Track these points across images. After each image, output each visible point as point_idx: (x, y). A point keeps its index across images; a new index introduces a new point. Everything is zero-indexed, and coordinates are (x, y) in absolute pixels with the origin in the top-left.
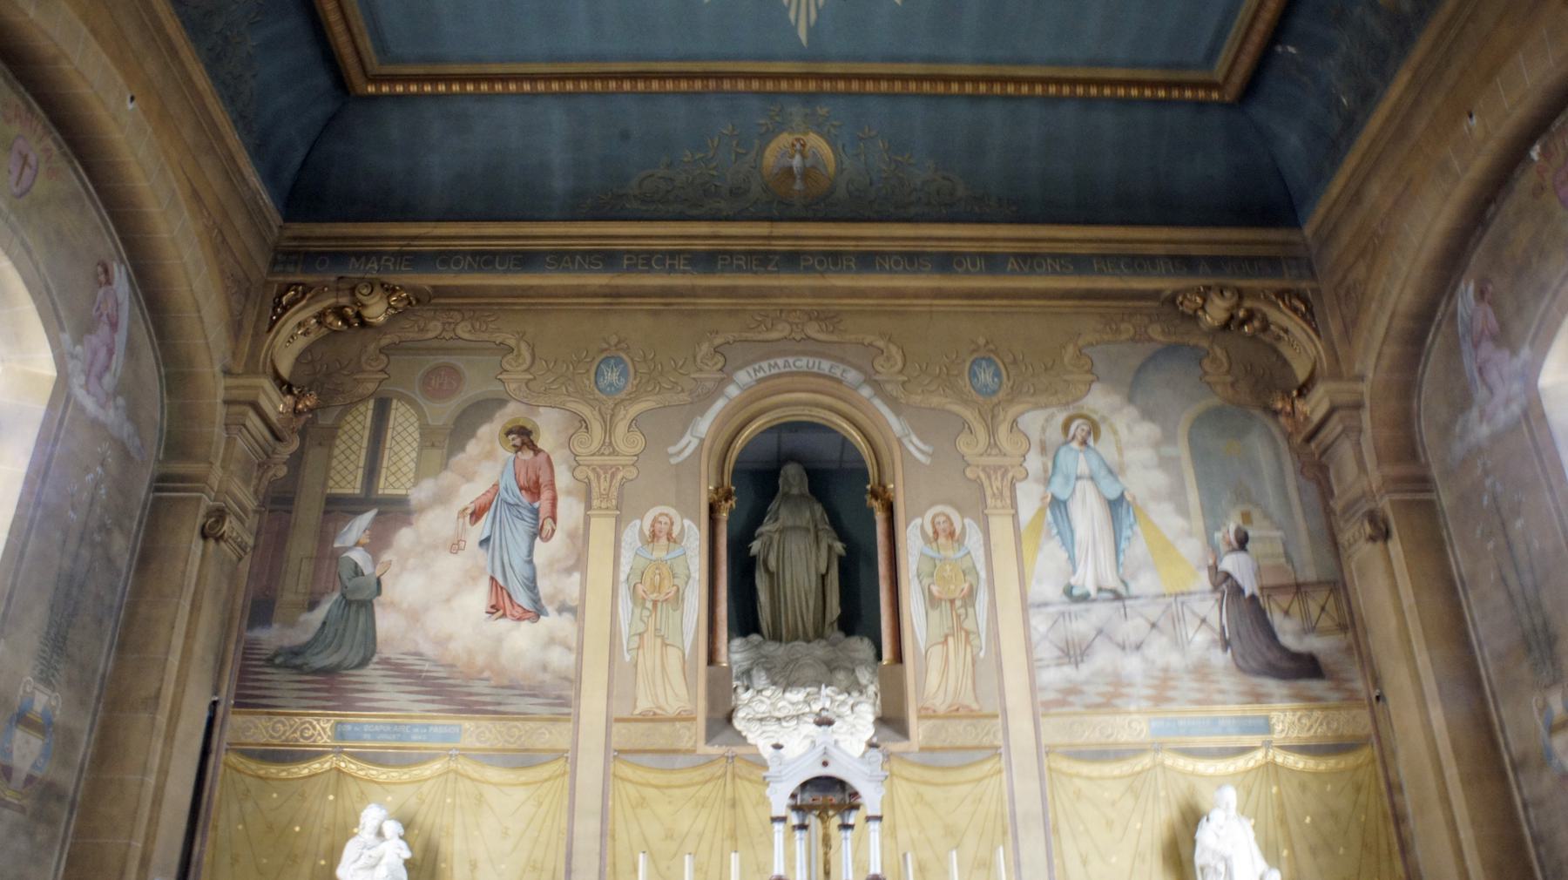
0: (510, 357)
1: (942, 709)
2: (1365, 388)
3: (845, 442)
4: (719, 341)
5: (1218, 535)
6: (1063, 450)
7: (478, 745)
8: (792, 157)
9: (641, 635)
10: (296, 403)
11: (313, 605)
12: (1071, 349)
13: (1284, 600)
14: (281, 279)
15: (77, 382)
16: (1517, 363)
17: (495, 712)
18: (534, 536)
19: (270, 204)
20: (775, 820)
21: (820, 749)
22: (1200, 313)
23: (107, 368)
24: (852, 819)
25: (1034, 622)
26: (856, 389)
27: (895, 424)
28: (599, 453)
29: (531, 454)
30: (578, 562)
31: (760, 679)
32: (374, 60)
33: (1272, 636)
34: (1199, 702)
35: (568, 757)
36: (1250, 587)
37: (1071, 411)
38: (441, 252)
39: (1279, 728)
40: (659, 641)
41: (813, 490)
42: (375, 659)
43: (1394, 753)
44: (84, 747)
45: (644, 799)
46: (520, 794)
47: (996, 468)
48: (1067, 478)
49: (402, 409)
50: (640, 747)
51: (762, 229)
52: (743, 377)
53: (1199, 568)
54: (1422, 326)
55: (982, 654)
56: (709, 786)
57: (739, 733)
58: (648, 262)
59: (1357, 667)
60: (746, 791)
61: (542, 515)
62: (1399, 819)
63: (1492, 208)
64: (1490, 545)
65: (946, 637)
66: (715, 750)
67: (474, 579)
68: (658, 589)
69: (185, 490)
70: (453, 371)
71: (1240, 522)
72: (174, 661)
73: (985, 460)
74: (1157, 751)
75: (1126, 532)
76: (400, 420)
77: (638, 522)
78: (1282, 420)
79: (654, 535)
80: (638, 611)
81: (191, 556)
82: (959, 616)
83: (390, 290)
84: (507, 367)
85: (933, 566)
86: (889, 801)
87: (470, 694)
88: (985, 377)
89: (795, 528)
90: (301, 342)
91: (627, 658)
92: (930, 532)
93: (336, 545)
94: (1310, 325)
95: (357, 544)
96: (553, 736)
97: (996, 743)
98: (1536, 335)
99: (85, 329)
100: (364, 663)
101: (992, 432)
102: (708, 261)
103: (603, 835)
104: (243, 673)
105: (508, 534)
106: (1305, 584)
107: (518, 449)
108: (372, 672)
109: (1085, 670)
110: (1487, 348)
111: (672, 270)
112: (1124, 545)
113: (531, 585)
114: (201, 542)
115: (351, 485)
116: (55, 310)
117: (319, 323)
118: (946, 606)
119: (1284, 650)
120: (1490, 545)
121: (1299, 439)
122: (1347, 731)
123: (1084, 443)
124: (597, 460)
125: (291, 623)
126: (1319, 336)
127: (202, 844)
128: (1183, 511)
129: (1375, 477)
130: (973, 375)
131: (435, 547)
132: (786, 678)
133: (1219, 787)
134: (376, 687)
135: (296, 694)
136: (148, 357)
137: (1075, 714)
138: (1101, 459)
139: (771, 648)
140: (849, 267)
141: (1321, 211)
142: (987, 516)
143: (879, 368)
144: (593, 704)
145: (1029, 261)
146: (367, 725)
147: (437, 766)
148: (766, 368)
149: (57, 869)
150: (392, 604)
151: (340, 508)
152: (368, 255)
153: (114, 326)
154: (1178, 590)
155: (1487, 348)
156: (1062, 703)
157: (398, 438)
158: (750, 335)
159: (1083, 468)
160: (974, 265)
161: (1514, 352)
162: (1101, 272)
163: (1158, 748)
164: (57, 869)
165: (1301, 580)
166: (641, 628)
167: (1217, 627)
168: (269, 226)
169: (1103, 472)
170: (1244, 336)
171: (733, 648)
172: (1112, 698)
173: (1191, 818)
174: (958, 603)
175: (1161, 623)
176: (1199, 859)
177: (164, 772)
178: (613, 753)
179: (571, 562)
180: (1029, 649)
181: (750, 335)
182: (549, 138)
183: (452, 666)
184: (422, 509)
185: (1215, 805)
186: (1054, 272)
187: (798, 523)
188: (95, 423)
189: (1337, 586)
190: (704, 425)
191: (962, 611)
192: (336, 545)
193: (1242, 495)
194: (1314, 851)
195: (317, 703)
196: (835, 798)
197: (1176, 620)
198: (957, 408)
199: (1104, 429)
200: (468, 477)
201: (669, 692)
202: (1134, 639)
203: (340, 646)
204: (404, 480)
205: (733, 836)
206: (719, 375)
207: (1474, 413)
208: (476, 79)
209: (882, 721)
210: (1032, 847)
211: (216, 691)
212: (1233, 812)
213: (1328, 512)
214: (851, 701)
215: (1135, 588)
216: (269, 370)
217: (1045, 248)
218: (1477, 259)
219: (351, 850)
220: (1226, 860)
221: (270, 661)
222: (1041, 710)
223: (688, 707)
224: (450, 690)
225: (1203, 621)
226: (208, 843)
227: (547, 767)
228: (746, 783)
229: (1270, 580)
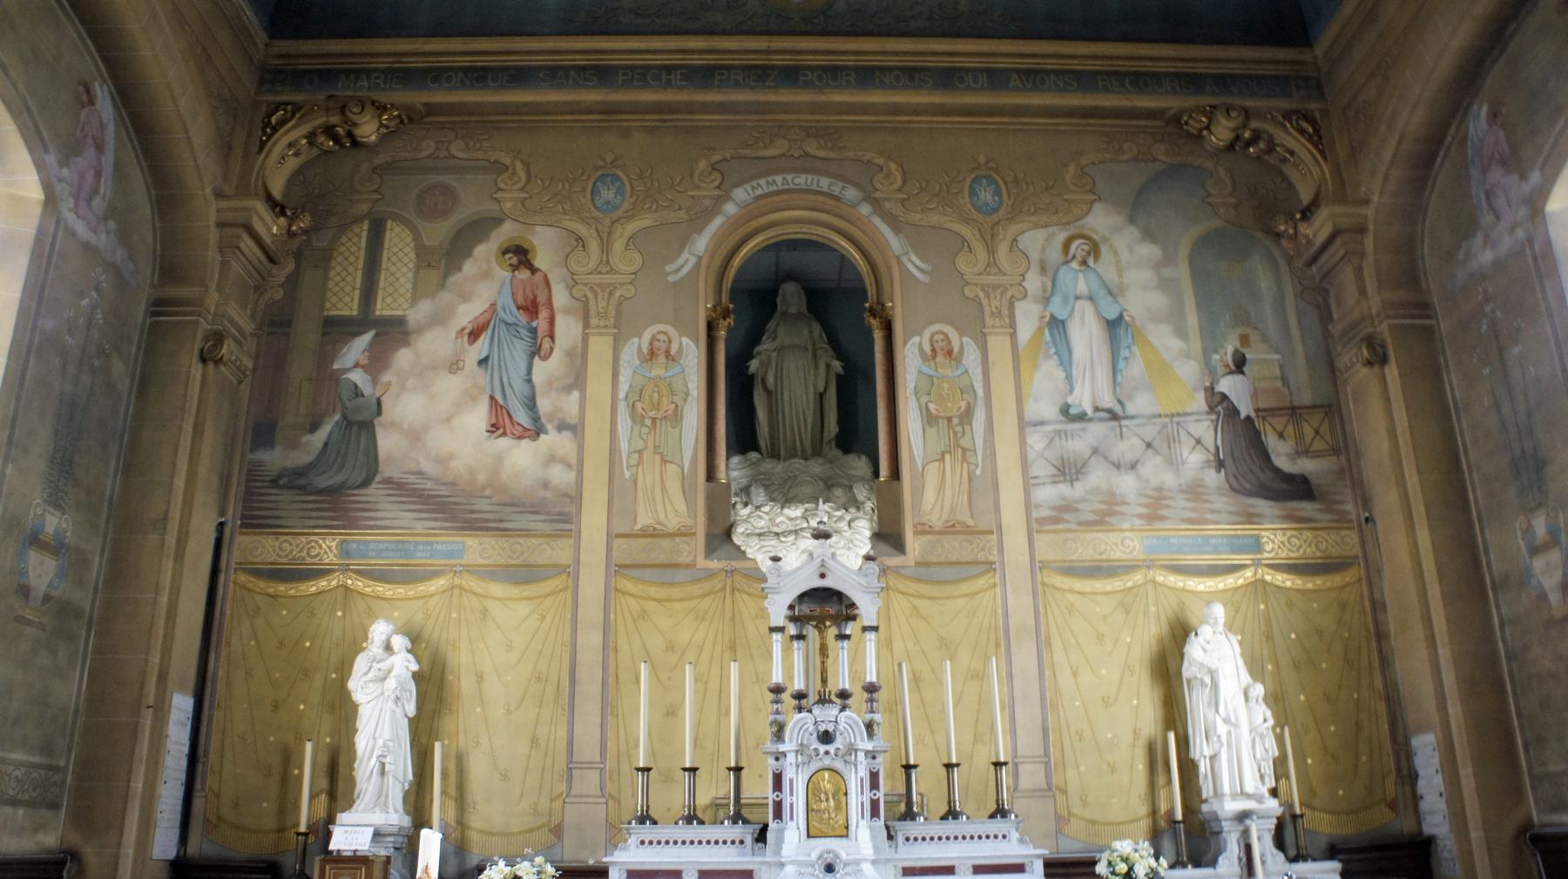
0: (505, 175)
1: (938, 525)
2: (1369, 212)
3: (844, 260)
4: (716, 158)
5: (1216, 357)
7: (482, 561)
9: (640, 452)
10: (290, 226)
11: (314, 427)
12: (1072, 168)
13: (1279, 422)
14: (270, 98)
15: (66, 205)
16: (1526, 188)
17: (498, 529)
18: (532, 355)
19: (255, 21)
20: (773, 630)
21: (817, 562)
22: (1205, 133)
23: (95, 192)
25: (1030, 440)
26: (854, 206)
27: (894, 242)
30: (577, 379)
31: (759, 495)
33: (1265, 456)
34: (1191, 521)
35: (571, 572)
36: (1245, 409)
37: (1072, 231)
40: (658, 458)
42: (378, 479)
43: (1379, 571)
44: (96, 569)
45: (645, 611)
46: (523, 608)
47: (995, 287)
48: (1066, 299)
49: (397, 230)
50: (640, 561)
52: (740, 194)
53: (1195, 389)
55: (978, 472)
56: (708, 600)
57: (738, 548)
58: (644, 75)
60: (746, 604)
61: (540, 334)
62: (1381, 636)
63: (1513, 27)
64: (1486, 371)
65: (943, 454)
66: (714, 564)
67: (474, 399)
68: (657, 407)
69: (177, 314)
71: (1238, 345)
72: (180, 483)
73: (986, 279)
74: (1148, 567)
75: (1124, 353)
76: (396, 240)
77: (636, 340)
78: (1284, 242)
79: (652, 353)
80: (637, 429)
82: (955, 433)
83: (381, 108)
84: (502, 185)
85: (930, 385)
86: (885, 612)
87: (472, 512)
88: (986, 195)
90: (292, 164)
91: (627, 475)
92: (928, 350)
94: (1315, 145)
95: (356, 365)
96: (559, 552)
97: (991, 558)
98: (1545, 162)
99: (70, 152)
100: (366, 483)
101: (991, 251)
102: (705, 75)
104: (249, 495)
105: (507, 352)
106: (1300, 408)
107: (515, 268)
108: (375, 492)
109: (1079, 490)
110: (1496, 175)
111: (668, 84)
112: (1121, 365)
113: (531, 404)
115: (348, 306)
116: (38, 131)
117: (310, 143)
118: (943, 423)
119: (1277, 471)
120: (1486, 371)
121: (1299, 263)
122: (1335, 551)
123: (1084, 263)
124: (595, 278)
125: (293, 445)
126: (1325, 158)
127: (217, 659)
128: (1181, 333)
129: (1375, 301)
130: (973, 193)
131: (434, 367)
132: (784, 494)
133: (1208, 603)
134: (380, 506)
135: (301, 513)
136: (138, 181)
137: (1070, 531)
138: (1100, 277)
139: (769, 465)
143: (878, 185)
144: (594, 521)
145: (1032, 77)
146: (373, 543)
147: (441, 582)
148: (764, 185)
149: (81, 681)
150: (394, 425)
151: (338, 330)
153: (100, 148)
155: (1496, 175)
156: (1056, 520)
157: (394, 259)
158: (747, 152)
159: (1082, 287)
160: (976, 82)
161: (1524, 177)
162: (1106, 90)
163: (1149, 565)
164: (81, 681)
165: (1296, 403)
166: (640, 445)
167: (1212, 449)
168: (255, 44)
169: (1103, 293)
170: (1249, 156)
171: (732, 466)
172: (1106, 515)
173: (1180, 632)
174: (955, 421)
175: (1155, 444)
176: (1186, 674)
177: (175, 591)
178: (614, 568)
179: (571, 380)
180: (1025, 465)
181: (747, 152)
183: (454, 484)
184: (420, 330)
185: (1204, 621)
188: (87, 246)
189: (1332, 409)
190: (702, 243)
191: (959, 429)
193: (1241, 318)
194: (1297, 666)
195: (321, 522)
196: (832, 609)
197: (1172, 440)
198: (956, 227)
199: (1104, 249)
200: (465, 297)
201: (669, 507)
202: (1129, 458)
203: (342, 467)
204: (401, 300)
205: (733, 647)
206: (716, 193)
207: (1478, 240)
209: (879, 536)
210: (1025, 658)
212: (1221, 628)
213: (1327, 335)
214: (848, 517)
215: (1131, 409)
216: (262, 193)
217: (1050, 64)
218: (1492, 81)
219: (360, 663)
220: (1212, 673)
221: (274, 482)
222: (1035, 526)
223: (688, 522)
225: (1198, 442)
226: (223, 660)
227: (550, 582)
228: (746, 598)
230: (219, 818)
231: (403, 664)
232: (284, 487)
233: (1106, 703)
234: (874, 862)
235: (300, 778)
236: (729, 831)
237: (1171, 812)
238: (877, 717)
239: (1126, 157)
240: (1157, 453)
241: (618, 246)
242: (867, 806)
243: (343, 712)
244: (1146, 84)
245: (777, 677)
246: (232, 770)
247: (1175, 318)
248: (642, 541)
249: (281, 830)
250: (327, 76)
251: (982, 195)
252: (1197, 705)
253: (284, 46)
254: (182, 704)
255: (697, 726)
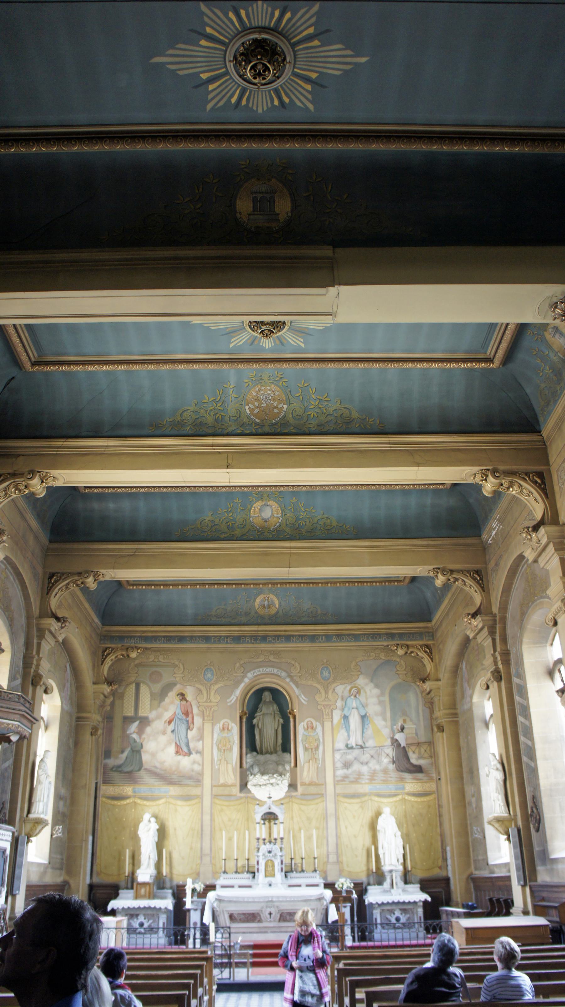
4: (242, 662)
5: (395, 727)
6: (349, 699)
9: (220, 760)
11: (123, 752)
13: (413, 748)
14: (103, 645)
24: (277, 822)
28: (206, 702)
29: (185, 702)
30: (201, 738)
35: (200, 797)
36: (403, 744)
38: (154, 637)
39: (407, 788)
41: (273, 699)
42: (143, 768)
47: (327, 705)
48: (349, 709)
49: (144, 687)
52: (250, 675)
54: (456, 670)
55: (320, 766)
57: (249, 790)
59: (434, 770)
62: (440, 816)
66: (242, 795)
70: (159, 674)
75: (366, 726)
79: (223, 729)
81: (87, 738)
84: (176, 672)
88: (326, 674)
89: (267, 714)
91: (217, 767)
92: (306, 727)
93: (128, 732)
95: (134, 732)
96: (195, 791)
101: (327, 693)
103: (211, 820)
104: (104, 773)
106: (421, 743)
108: (142, 773)
109: (350, 771)
112: (365, 730)
113: (188, 745)
114: (91, 737)
115: (130, 712)
118: (310, 750)
119: (412, 764)
121: (424, 694)
123: (355, 696)
124: (206, 704)
125: (117, 758)
128: (385, 719)
130: (322, 673)
140: (282, 641)
142: (323, 722)
143: (292, 671)
144: (207, 782)
146: (142, 789)
147: (163, 801)
148: (257, 672)
151: (128, 720)
152: (131, 637)
154: (380, 745)
156: (342, 781)
158: (251, 660)
162: (363, 641)
165: (420, 741)
169: (361, 706)
170: (412, 656)
173: (378, 814)
174: (314, 750)
181: (251, 660)
183: (166, 770)
184: (153, 721)
186: (348, 641)
187: (268, 712)
189: (431, 743)
191: (314, 752)
192: (128, 732)
193: (404, 714)
196: (273, 817)
197: (379, 755)
198: (316, 685)
199: (362, 691)
200: (166, 710)
202: (366, 761)
203: (132, 765)
206: (242, 675)
210: (332, 823)
211: (97, 779)
215: (367, 745)
221: (112, 769)
222: (336, 782)
224: (166, 777)
229: (410, 742)
230: (101, 871)
231: (154, 826)
232: (116, 771)
233: (355, 837)
234: (282, 884)
235: (125, 860)
236: (246, 875)
237: (372, 870)
238: (283, 846)
239: (371, 658)
240: (374, 758)
241: (212, 693)
242: (280, 869)
243: (136, 839)
244: (376, 638)
245: (258, 836)
246: (103, 857)
247: (383, 714)
248: (221, 788)
249: (119, 875)
250: (121, 638)
251: (324, 673)
252: (381, 838)
253: (107, 628)
254: (91, 838)
255: (238, 843)
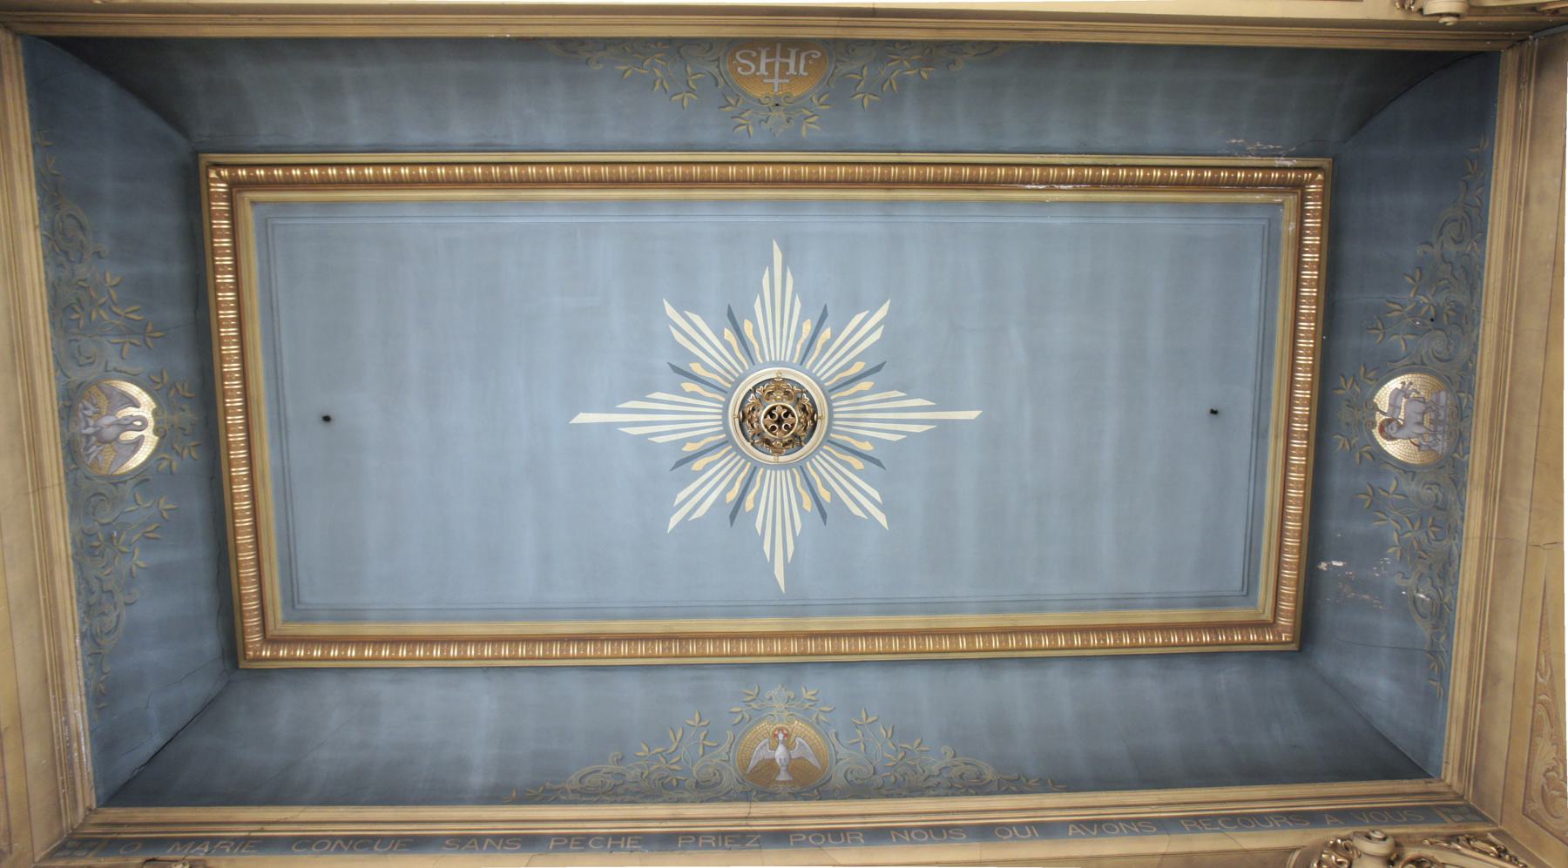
8: (774, 749)
32: (280, 616)
51: (740, 809)
141: (1454, 736)
152: (199, 841)
168: (75, 801)
182: (473, 719)
208: (395, 642)
